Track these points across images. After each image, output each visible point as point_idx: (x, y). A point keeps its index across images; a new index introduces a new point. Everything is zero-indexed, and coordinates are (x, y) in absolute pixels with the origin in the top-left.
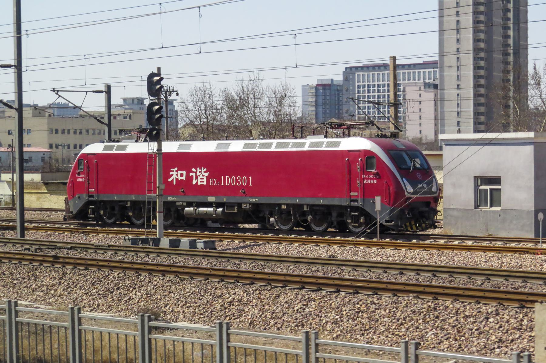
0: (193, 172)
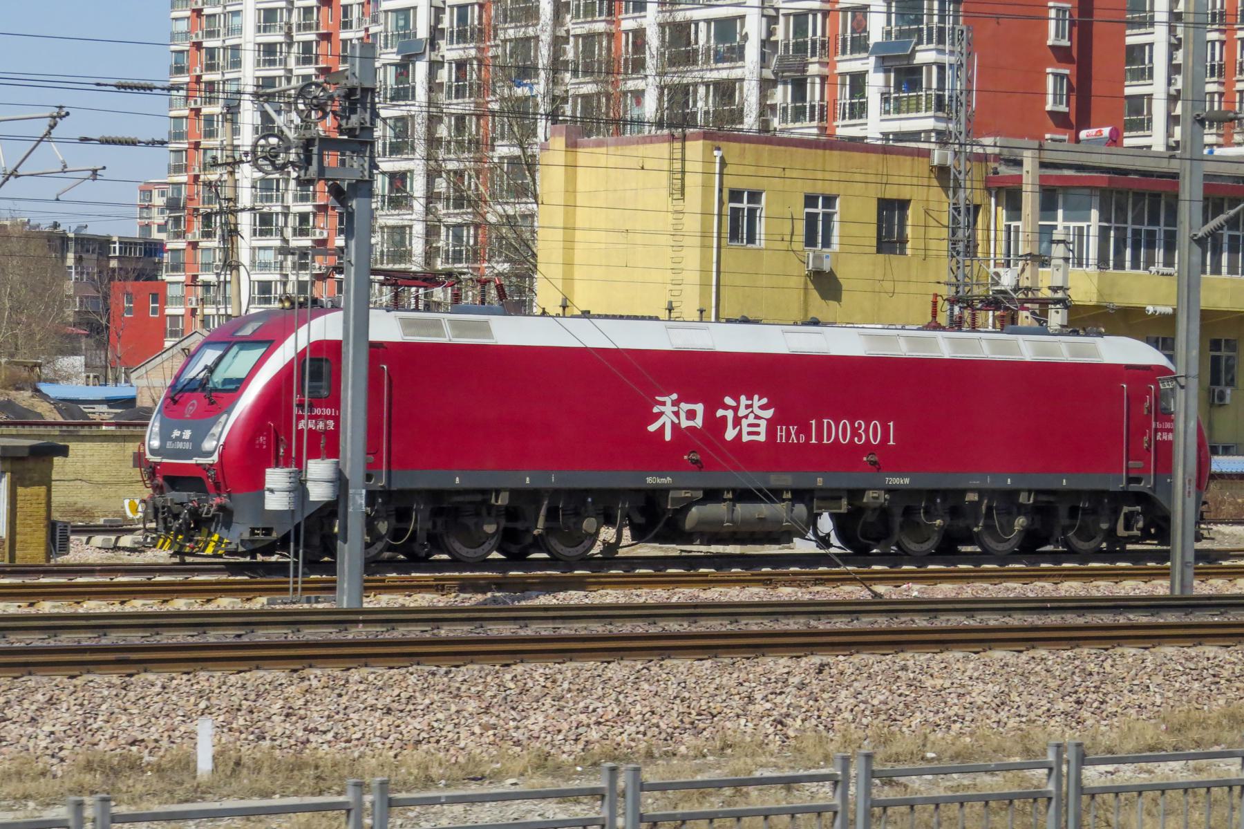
0: (726, 407)
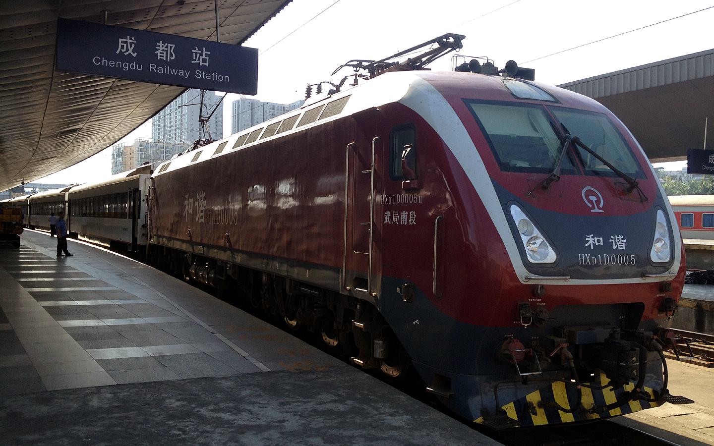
0: (613, 239)
